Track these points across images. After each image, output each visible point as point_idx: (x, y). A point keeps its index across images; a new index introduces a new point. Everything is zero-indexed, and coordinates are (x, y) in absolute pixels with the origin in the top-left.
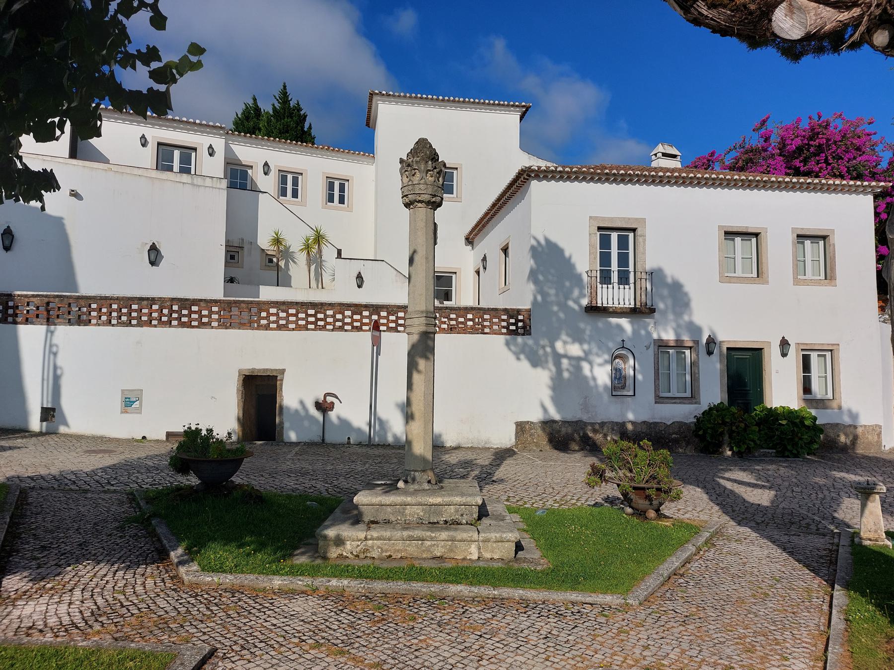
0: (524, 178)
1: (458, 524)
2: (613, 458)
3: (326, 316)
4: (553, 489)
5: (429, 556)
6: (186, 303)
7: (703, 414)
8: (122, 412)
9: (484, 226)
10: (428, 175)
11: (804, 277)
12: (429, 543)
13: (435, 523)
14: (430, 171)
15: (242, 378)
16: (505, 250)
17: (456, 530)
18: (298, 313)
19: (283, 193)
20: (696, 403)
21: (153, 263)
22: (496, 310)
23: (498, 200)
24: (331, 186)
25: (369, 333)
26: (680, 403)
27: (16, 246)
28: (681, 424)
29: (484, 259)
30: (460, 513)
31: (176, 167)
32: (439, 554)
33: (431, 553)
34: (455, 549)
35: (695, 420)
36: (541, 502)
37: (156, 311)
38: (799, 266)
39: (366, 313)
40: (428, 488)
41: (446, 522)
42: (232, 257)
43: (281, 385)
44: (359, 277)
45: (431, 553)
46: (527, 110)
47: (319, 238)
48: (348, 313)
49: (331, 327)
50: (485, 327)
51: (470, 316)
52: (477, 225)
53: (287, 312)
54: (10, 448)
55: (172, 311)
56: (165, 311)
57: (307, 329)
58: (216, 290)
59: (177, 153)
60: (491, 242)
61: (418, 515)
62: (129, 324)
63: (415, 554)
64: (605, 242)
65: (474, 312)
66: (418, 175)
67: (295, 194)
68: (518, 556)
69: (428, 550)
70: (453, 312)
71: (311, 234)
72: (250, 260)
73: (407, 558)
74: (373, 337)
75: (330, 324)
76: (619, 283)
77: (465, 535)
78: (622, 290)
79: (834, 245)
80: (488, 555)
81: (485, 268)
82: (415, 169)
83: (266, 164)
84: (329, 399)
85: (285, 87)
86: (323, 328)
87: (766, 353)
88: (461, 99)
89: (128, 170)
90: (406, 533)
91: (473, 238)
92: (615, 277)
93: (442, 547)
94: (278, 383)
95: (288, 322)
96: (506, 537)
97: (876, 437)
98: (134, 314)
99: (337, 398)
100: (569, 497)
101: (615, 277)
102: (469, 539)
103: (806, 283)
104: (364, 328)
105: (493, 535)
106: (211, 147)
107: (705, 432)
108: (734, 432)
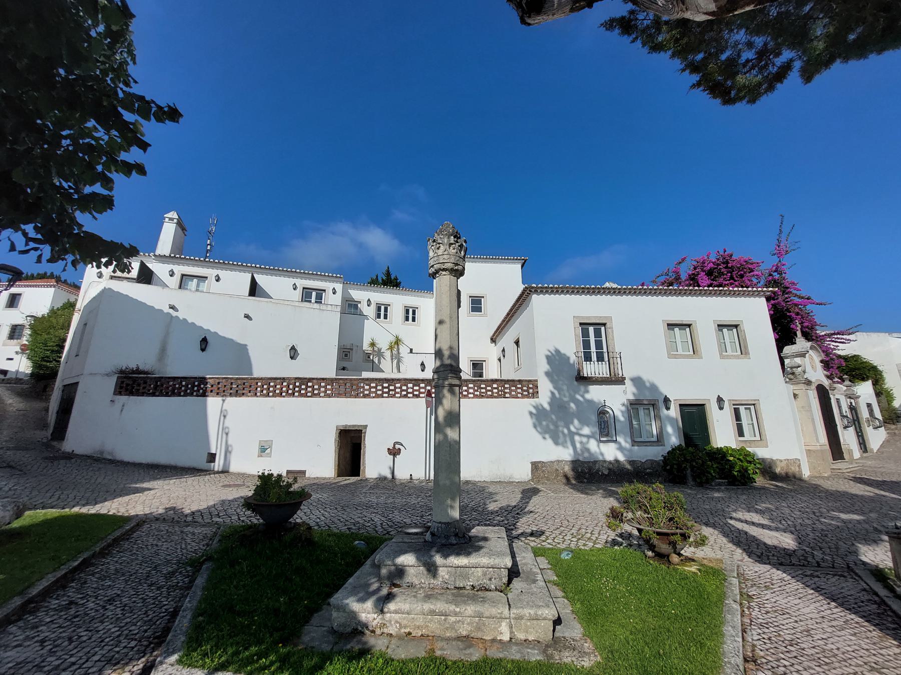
0: (528, 293)
1: (487, 590)
2: (630, 501)
3: (396, 388)
4: (568, 521)
5: (454, 635)
6: (304, 381)
7: (668, 453)
8: (258, 456)
9: (502, 329)
10: (451, 248)
11: (726, 354)
12: (453, 619)
13: (461, 588)
14: (452, 244)
15: (338, 432)
16: (517, 343)
17: (484, 600)
18: (377, 386)
19: (379, 316)
20: (661, 445)
21: (292, 358)
22: (513, 381)
23: (511, 310)
24: (407, 312)
25: (424, 399)
26: (650, 446)
27: (209, 349)
28: (652, 462)
29: (503, 350)
30: (488, 576)
31: (313, 300)
32: (464, 633)
33: (456, 631)
34: (483, 627)
35: (663, 458)
36: (561, 537)
37: (285, 386)
38: (722, 347)
39: (422, 385)
40: (455, 542)
41: (473, 587)
42: (346, 355)
43: (365, 436)
44: (422, 364)
45: (456, 631)
46: (525, 262)
47: (398, 342)
48: (410, 385)
49: (399, 395)
50: (506, 393)
51: (495, 386)
52: (497, 330)
53: (370, 385)
54: (150, 489)
55: (295, 386)
56: (291, 387)
57: (383, 397)
58: (330, 372)
59: (314, 294)
60: (507, 340)
61: (443, 578)
62: (268, 395)
63: (438, 632)
64: (585, 334)
65: (498, 383)
66: (442, 248)
67: (386, 317)
68: (557, 634)
69: (452, 627)
70: (483, 383)
71: (393, 339)
72: (356, 357)
73: (428, 636)
74: (427, 402)
75: (398, 393)
76: (598, 361)
77: (494, 611)
78: (600, 365)
79: (744, 330)
80: (521, 636)
81: (504, 356)
82: (439, 243)
83: (369, 300)
84: (397, 446)
85: (388, 268)
86: (394, 396)
87: (707, 407)
88: (485, 257)
89: (282, 302)
90: (427, 606)
91: (496, 339)
92: (594, 357)
93: (468, 624)
94: (363, 435)
95: (370, 392)
96: (542, 614)
97: (797, 469)
98: (271, 389)
99: (402, 445)
100: (584, 530)
101: (594, 357)
102: (499, 616)
103: (728, 357)
104: (421, 395)
105: (527, 612)
106: (334, 289)
107: (672, 467)
108: (695, 467)
